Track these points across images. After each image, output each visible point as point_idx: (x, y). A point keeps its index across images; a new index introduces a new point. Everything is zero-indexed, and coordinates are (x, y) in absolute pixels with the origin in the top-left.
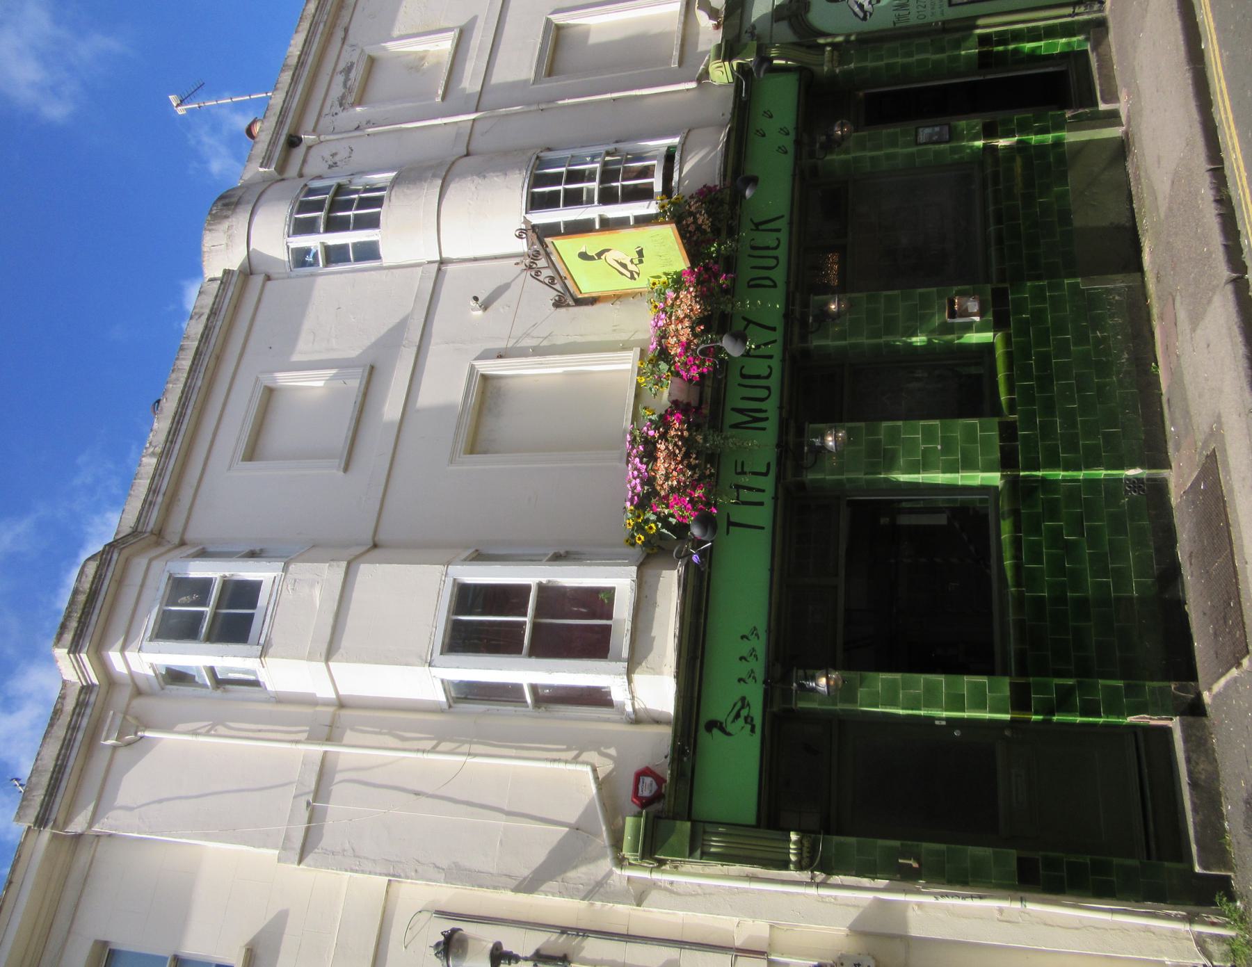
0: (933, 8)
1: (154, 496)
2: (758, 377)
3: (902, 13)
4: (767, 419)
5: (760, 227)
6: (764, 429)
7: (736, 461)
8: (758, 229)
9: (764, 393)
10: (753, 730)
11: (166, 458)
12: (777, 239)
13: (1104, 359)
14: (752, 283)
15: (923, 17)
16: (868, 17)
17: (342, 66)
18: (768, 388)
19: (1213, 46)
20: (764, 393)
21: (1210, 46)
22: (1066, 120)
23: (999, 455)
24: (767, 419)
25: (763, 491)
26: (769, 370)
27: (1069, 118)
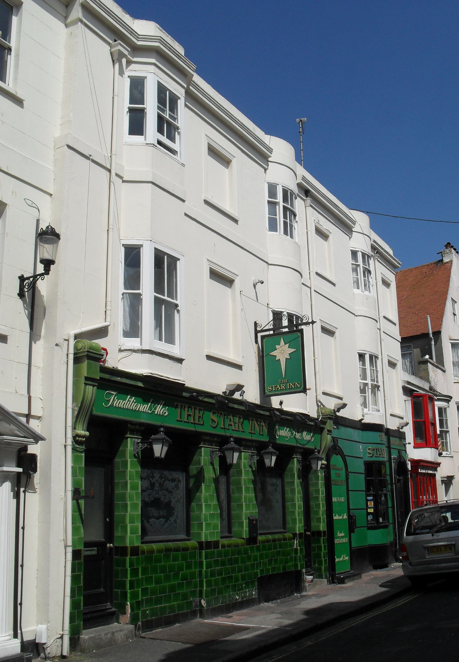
23: (209, 541)
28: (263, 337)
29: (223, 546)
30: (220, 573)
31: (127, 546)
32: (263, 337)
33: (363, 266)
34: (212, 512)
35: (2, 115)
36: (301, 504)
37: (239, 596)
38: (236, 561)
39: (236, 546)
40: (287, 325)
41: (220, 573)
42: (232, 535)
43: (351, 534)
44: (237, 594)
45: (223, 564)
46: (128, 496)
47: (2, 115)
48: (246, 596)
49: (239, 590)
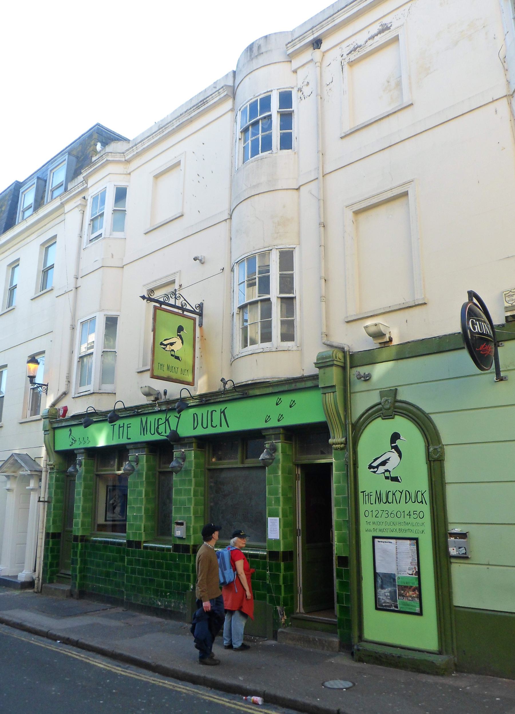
0: (374, 523)
1: (187, 114)
2: (212, 421)
3: (373, 498)
4: (144, 435)
5: (222, 414)
6: (141, 435)
7: (130, 424)
8: (221, 413)
9: (205, 426)
10: (71, 445)
11: (196, 108)
12: (216, 426)
13: (159, 594)
14: (195, 415)
15: (367, 515)
16: (372, 470)
17: (385, 21)
18: (207, 427)
19: (134, 674)
20: (205, 426)
21: (134, 673)
22: (276, 605)
23: (131, 540)
24: (144, 435)
25: (228, 427)
26: (215, 426)
27: (276, 608)
28: (194, 320)
29: (146, 548)
30: (141, 573)
31: (283, 562)
32: (194, 320)
33: (258, 99)
34: (135, 514)
35: (112, 255)
36: (76, 496)
37: (162, 603)
38: (160, 566)
39: (120, 544)
40: (468, 301)
41: (141, 573)
42: (348, 568)
43: (235, 565)
44: (160, 600)
45: (145, 564)
46: (144, 503)
47: (112, 255)
48: (170, 606)
49: (162, 596)
